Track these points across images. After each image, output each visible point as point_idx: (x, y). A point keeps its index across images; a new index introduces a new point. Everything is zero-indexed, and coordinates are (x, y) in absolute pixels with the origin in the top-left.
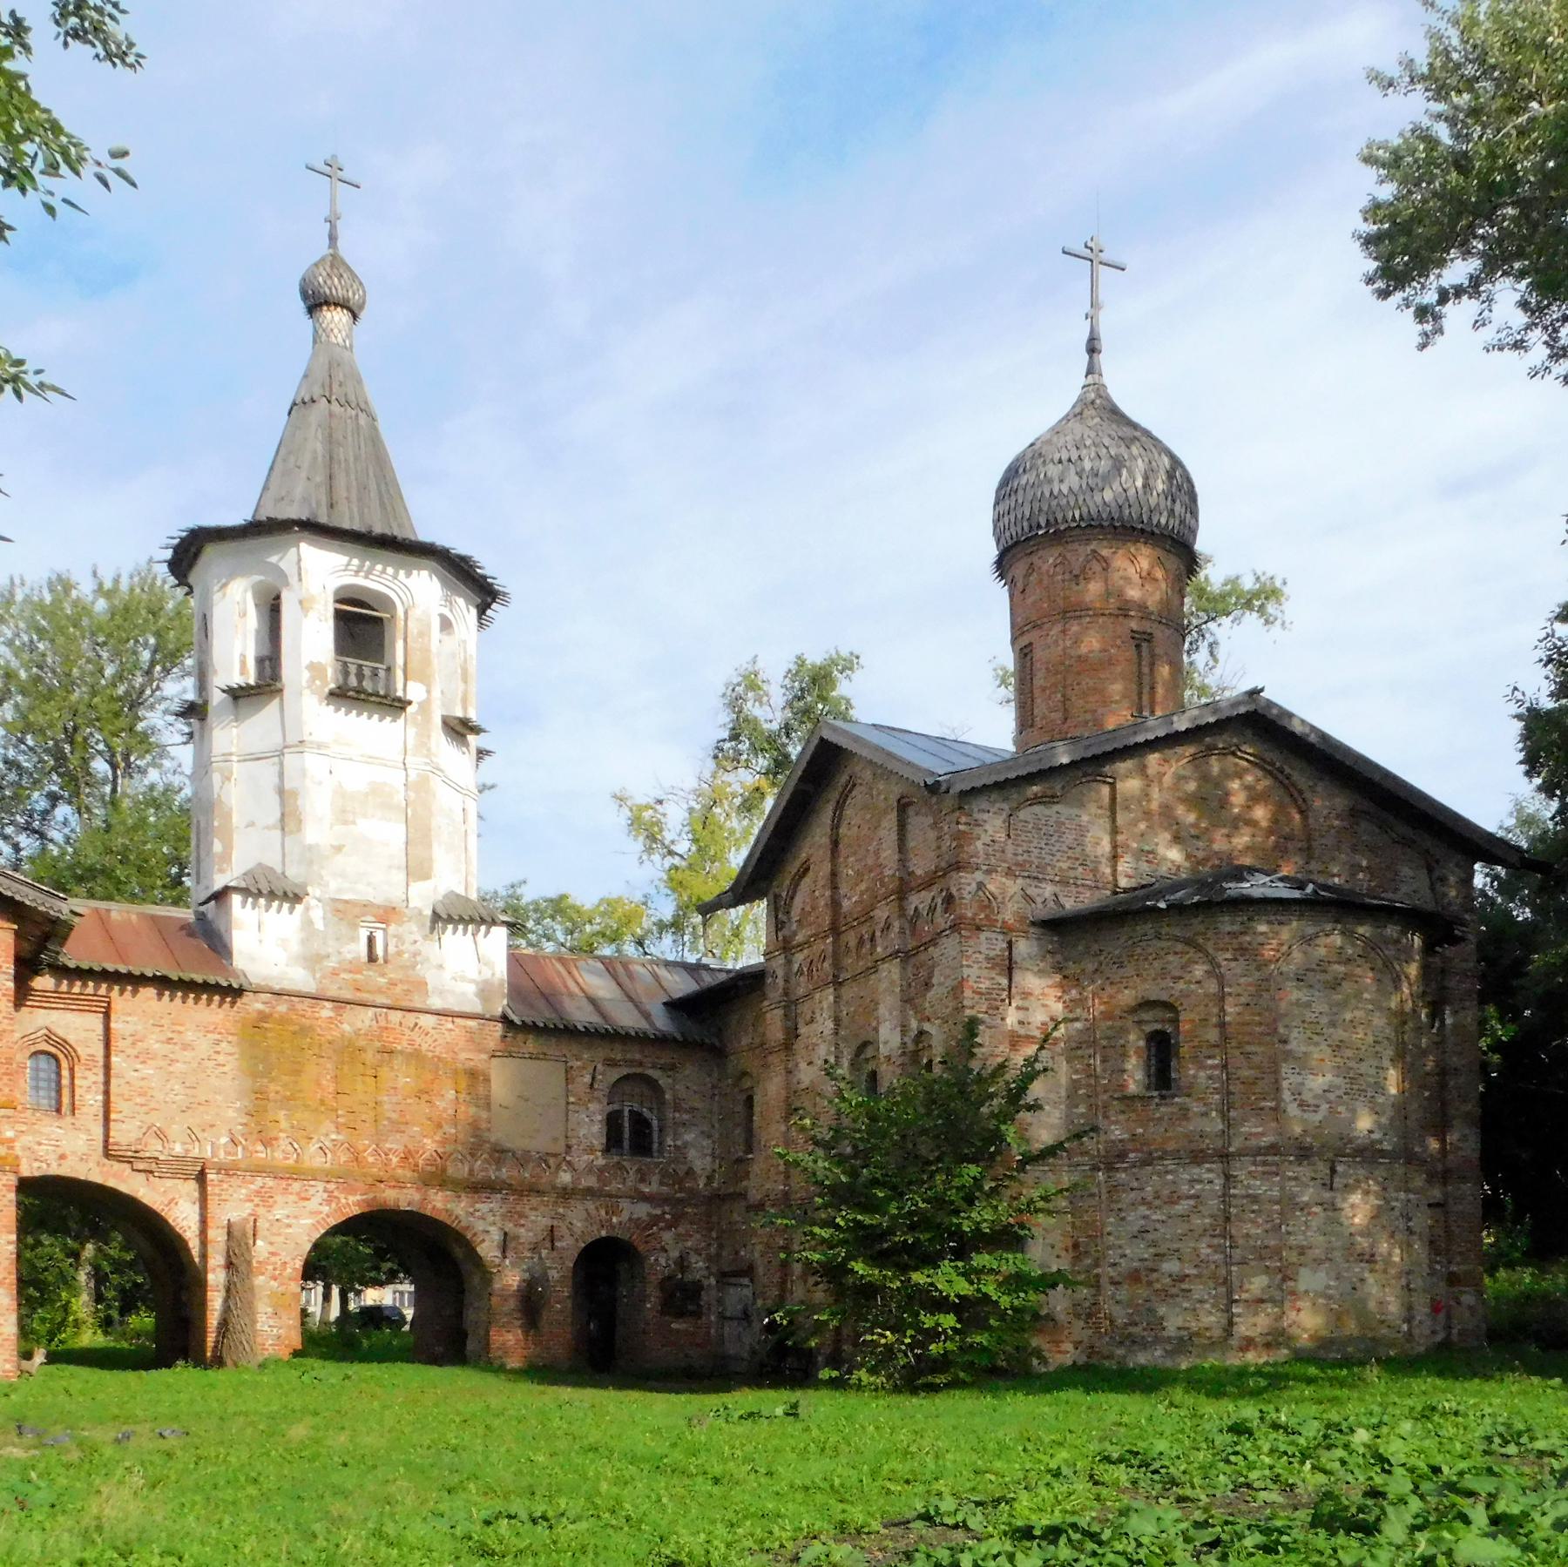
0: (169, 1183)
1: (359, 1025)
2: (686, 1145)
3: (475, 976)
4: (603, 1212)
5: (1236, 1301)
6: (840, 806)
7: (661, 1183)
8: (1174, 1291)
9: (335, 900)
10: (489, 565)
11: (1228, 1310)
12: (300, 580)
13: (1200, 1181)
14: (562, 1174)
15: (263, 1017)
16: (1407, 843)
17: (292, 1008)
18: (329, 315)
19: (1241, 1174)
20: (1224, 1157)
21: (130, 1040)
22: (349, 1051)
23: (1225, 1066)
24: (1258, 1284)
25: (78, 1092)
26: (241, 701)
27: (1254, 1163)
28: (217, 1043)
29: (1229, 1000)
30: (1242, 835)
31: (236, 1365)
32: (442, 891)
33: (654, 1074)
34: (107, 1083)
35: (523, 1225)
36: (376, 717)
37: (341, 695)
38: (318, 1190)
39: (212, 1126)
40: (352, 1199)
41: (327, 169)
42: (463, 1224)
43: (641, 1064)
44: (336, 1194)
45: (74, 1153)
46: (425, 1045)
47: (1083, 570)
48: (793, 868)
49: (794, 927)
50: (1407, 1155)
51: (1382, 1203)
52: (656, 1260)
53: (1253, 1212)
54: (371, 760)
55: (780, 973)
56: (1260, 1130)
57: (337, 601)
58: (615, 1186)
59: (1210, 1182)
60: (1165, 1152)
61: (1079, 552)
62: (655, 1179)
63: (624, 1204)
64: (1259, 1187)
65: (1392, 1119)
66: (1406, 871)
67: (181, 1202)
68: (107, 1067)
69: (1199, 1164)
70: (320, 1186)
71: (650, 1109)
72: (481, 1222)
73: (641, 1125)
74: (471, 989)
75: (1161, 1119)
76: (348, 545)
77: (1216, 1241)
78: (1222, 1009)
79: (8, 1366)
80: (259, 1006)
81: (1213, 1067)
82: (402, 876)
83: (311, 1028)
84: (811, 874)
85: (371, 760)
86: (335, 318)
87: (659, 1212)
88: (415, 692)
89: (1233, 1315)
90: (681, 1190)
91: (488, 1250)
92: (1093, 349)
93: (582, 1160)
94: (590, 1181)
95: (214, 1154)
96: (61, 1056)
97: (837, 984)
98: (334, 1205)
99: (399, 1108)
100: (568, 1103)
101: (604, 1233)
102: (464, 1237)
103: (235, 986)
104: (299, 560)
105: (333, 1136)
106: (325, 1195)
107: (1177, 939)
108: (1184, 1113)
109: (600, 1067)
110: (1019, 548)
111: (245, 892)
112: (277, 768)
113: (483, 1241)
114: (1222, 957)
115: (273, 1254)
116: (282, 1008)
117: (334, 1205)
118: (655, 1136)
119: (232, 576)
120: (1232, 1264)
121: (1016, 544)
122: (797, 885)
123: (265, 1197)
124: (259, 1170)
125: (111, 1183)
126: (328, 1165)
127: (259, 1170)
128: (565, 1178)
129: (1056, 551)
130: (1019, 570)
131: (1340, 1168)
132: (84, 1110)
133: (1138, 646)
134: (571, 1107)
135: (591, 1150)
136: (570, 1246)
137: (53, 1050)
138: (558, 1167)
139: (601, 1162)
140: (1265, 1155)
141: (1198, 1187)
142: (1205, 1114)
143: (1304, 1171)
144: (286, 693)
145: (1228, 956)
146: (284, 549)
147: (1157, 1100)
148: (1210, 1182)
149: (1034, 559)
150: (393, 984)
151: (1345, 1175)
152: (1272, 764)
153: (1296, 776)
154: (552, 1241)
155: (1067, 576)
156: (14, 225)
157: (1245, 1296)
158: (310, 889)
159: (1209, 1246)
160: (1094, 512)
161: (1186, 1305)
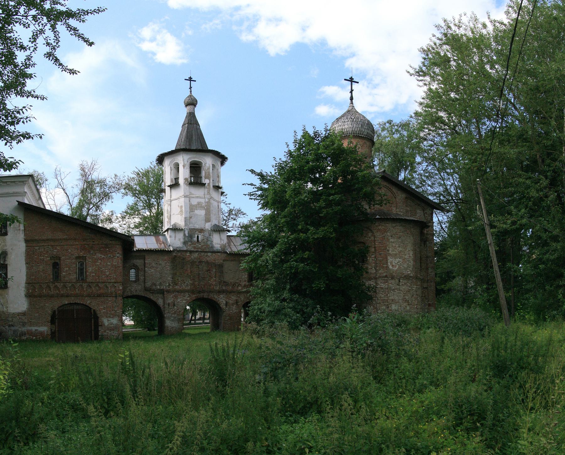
0: (157, 295)
3: (220, 243)
10: (223, 153)
15: (175, 256)
16: (419, 205)
20: (376, 278)
22: (193, 263)
23: (375, 257)
28: (166, 263)
29: (376, 241)
31: (138, 174)
32: (213, 224)
37: (191, 184)
50: (416, 278)
51: (312, 135)
54: (197, 197)
64: (383, 285)
65: (413, 268)
66: (418, 211)
69: (370, 280)
74: (219, 246)
80: (174, 254)
82: (204, 222)
83: (185, 258)
85: (197, 197)
88: (206, 181)
91: (223, 306)
95: (166, 288)
116: (179, 254)
123: (176, 297)
125: (146, 296)
131: (401, 280)
135: (245, 281)
138: (238, 286)
139: (247, 284)
142: (372, 268)
143: (393, 281)
151: (402, 282)
153: (393, 190)
154: (237, 303)
156: (103, 6)
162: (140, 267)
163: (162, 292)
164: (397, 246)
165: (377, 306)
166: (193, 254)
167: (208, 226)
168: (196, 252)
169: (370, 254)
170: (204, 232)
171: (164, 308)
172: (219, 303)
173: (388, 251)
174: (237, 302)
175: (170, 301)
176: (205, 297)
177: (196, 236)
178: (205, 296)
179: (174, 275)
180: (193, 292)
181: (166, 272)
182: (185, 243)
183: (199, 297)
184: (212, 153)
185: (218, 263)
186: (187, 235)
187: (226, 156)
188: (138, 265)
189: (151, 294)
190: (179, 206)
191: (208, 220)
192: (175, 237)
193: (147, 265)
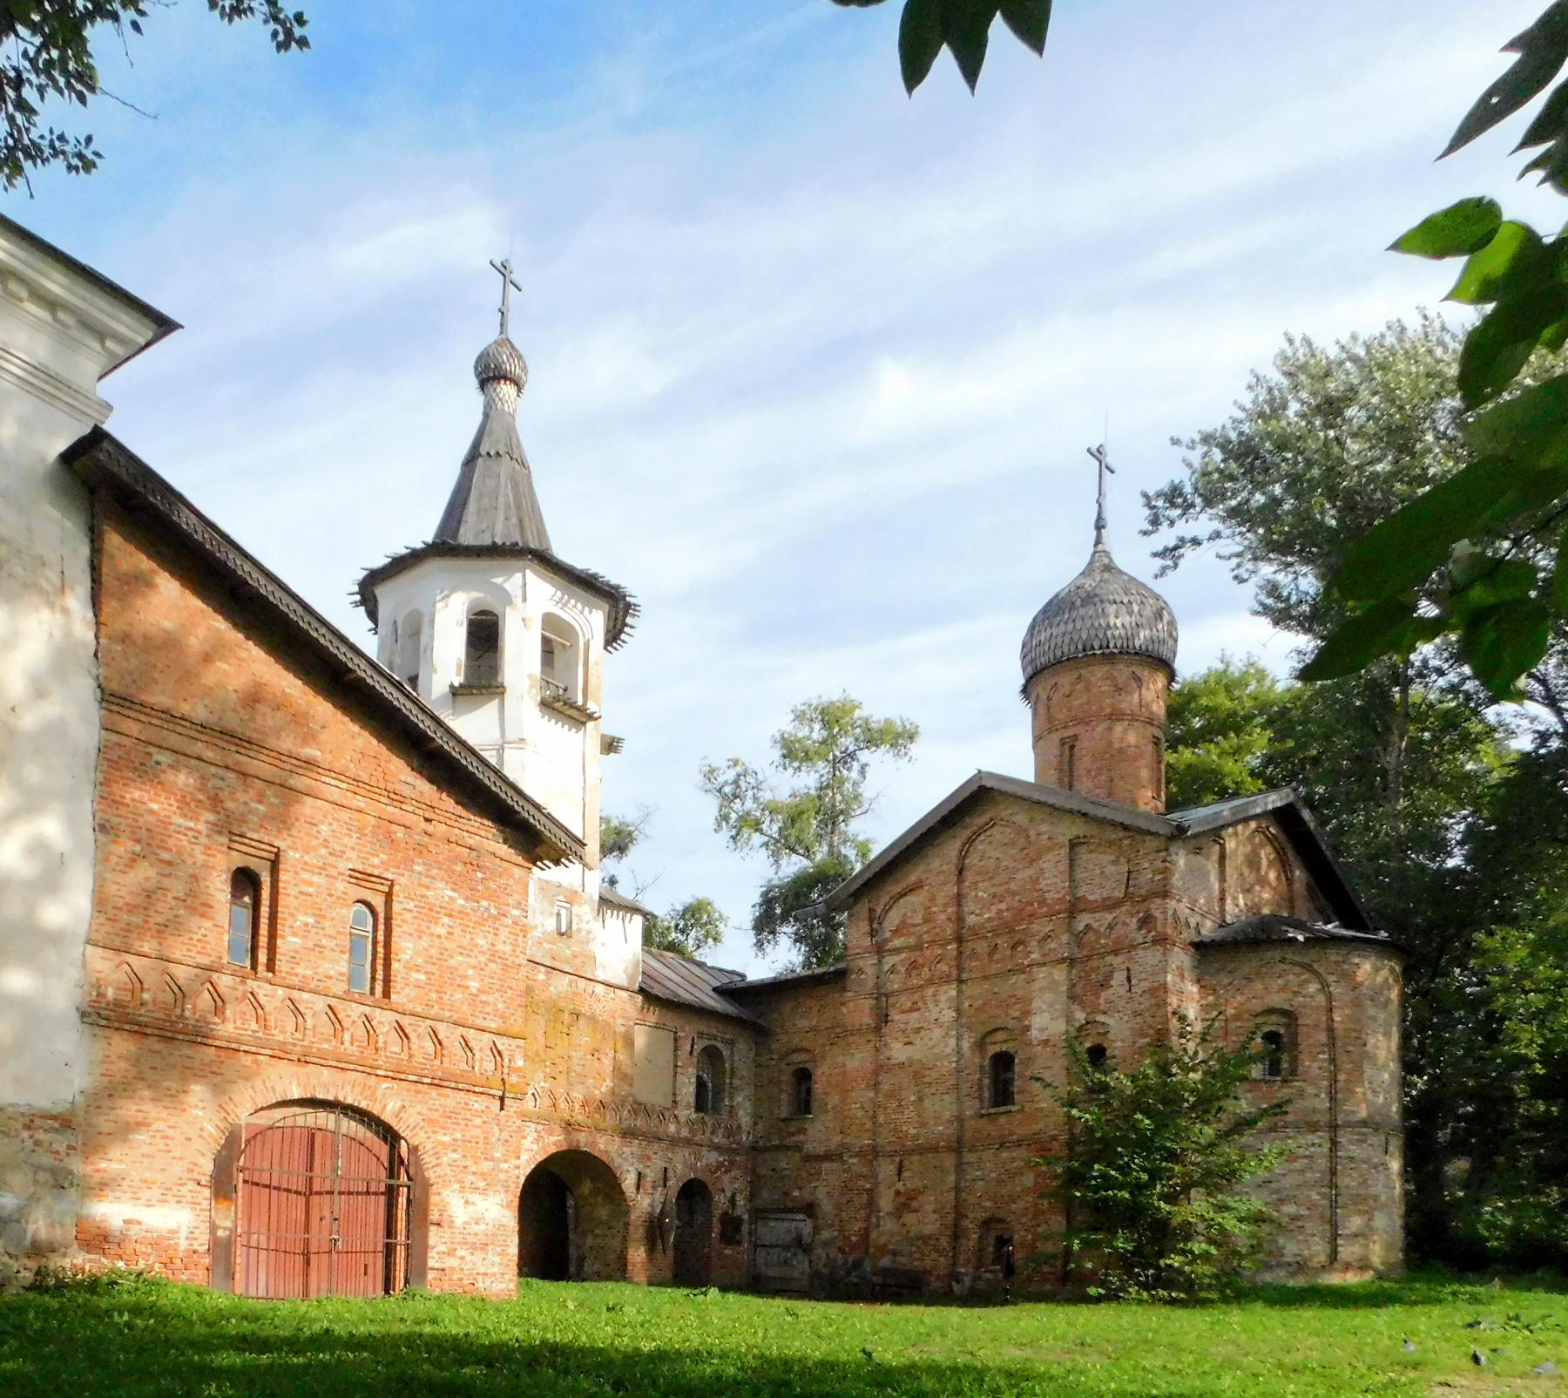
1: (560, 988)
6: (970, 841)
8: (1292, 1227)
12: (525, 600)
18: (504, 387)
24: (1356, 1223)
36: (566, 727)
41: (502, 269)
46: (598, 1009)
49: (888, 934)
55: (870, 971)
61: (1122, 672)
62: (720, 1135)
63: (705, 1152)
69: (1313, 1132)
70: (533, 1126)
81: (1323, 1060)
86: (507, 390)
92: (1100, 525)
94: (685, 1133)
97: (960, 981)
100: (676, 1066)
104: (525, 585)
107: (1295, 964)
108: (1301, 1093)
119: (454, 590)
130: (1041, 689)
135: (688, 1107)
136: (674, 1184)
139: (694, 1116)
141: (1312, 1149)
144: (509, 696)
145: (1334, 978)
146: (509, 573)
157: (1347, 1232)
159: (1319, 1194)
161: (1301, 1238)
173: (1365, 1045)
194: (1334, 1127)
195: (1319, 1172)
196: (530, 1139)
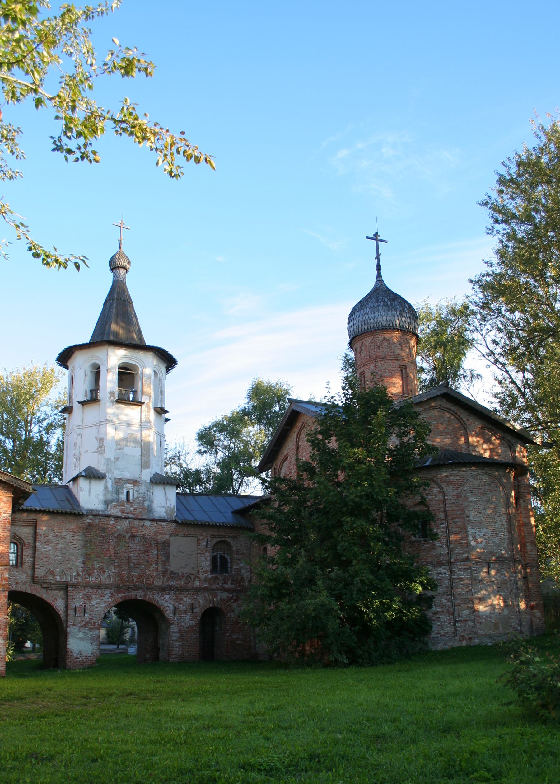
0: (54, 592)
1: (123, 526)
2: (241, 568)
3: (164, 505)
4: (211, 597)
5: (457, 621)
6: (299, 434)
7: (232, 584)
8: (433, 618)
9: (115, 478)
11: (454, 625)
13: (441, 573)
14: (196, 582)
17: (100, 521)
19: (456, 570)
21: (43, 536)
22: (120, 537)
25: (24, 557)
26: (85, 406)
27: (460, 565)
28: (73, 536)
29: (447, 502)
30: (487, 441)
32: (153, 472)
33: (229, 540)
34: (34, 553)
35: (181, 603)
38: (107, 593)
39: (71, 569)
40: (120, 596)
42: (160, 604)
43: (224, 536)
44: (114, 594)
45: (21, 581)
47: (381, 344)
48: (281, 458)
52: (230, 615)
53: (461, 584)
56: (462, 552)
57: (119, 368)
58: (215, 586)
59: (445, 573)
60: (427, 562)
62: (230, 582)
67: (58, 599)
68: (35, 548)
69: (440, 567)
70: (108, 591)
71: (227, 554)
72: (166, 603)
73: (224, 561)
74: (164, 510)
75: (425, 549)
76: (133, 350)
77: (448, 597)
78: (445, 505)
79: (2, 669)
80: (88, 521)
81: (443, 528)
82: (139, 468)
83: (107, 528)
84: (288, 459)
87: (231, 596)
89: (456, 627)
90: (239, 586)
91: (169, 614)
93: (203, 576)
94: (206, 585)
96: (19, 544)
98: (113, 599)
99: (137, 558)
101: (211, 605)
102: (160, 609)
103: (81, 513)
105: (114, 571)
106: (110, 595)
108: (434, 547)
109: (210, 539)
110: (358, 337)
111: (86, 477)
112: (97, 430)
113: (167, 610)
114: (443, 485)
115: (91, 619)
117: (113, 599)
118: (229, 564)
120: (455, 606)
121: (357, 336)
122: (283, 463)
123: (88, 597)
124: (87, 585)
125: (34, 593)
126: (111, 582)
127: (87, 585)
128: (197, 583)
129: (371, 338)
130: (357, 345)
132: (26, 564)
133: (401, 370)
134: (199, 555)
135: (206, 572)
136: (199, 610)
137: (16, 541)
138: (194, 579)
139: (210, 576)
140: (464, 561)
141: (441, 576)
142: (441, 547)
145: (445, 484)
147: (423, 542)
148: (445, 573)
149: (363, 341)
150: (135, 509)
152: (453, 411)
153: (462, 416)
155: (376, 347)
157: (460, 619)
158: (107, 475)
159: (446, 599)
160: (384, 324)
162: (26, 541)
163: (65, 587)
164: (481, 507)
165: (454, 609)
166: (119, 522)
167: (146, 475)
168: (126, 518)
169: (438, 523)
170: (138, 486)
171: (67, 616)
172: (162, 608)
173: (468, 517)
174: (192, 607)
175: (78, 604)
176: (138, 598)
177: (125, 491)
178: (139, 595)
179: (87, 558)
180: (118, 589)
181: (72, 551)
182: (107, 503)
183: (128, 598)
184: (155, 353)
185: (162, 540)
186: (110, 488)
187: (176, 357)
188: (23, 536)
189: (44, 590)
190: (96, 439)
191: (145, 464)
192: (89, 491)
193: (39, 538)
194: (450, 563)
195: (446, 587)
196: (107, 597)
